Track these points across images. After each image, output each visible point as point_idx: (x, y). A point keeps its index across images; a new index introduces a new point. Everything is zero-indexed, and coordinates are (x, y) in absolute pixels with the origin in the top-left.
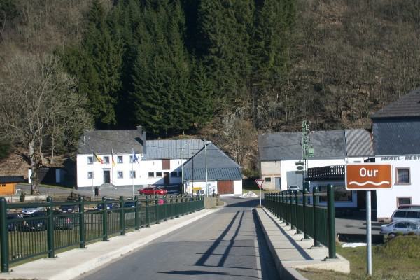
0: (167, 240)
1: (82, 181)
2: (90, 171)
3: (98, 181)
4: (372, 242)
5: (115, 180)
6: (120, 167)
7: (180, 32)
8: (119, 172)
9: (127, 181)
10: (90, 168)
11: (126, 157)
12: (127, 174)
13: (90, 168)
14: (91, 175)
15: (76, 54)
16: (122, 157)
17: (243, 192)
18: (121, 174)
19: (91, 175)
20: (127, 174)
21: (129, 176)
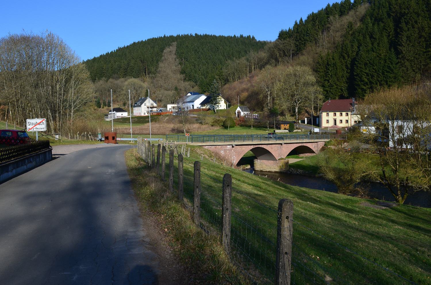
0: (298, 163)
1: (324, 124)
2: (327, 119)
3: (331, 124)
4: (337, 192)
5: (339, 124)
6: (341, 118)
7: (357, 200)
8: (327, 120)
9: (344, 125)
10: (327, 118)
11: (344, 113)
12: (344, 121)
13: (327, 118)
14: (328, 121)
15: (376, 57)
16: (336, 113)
17: (288, 160)
18: (341, 121)
19: (328, 121)
20: (344, 121)
21: (339, 122)
